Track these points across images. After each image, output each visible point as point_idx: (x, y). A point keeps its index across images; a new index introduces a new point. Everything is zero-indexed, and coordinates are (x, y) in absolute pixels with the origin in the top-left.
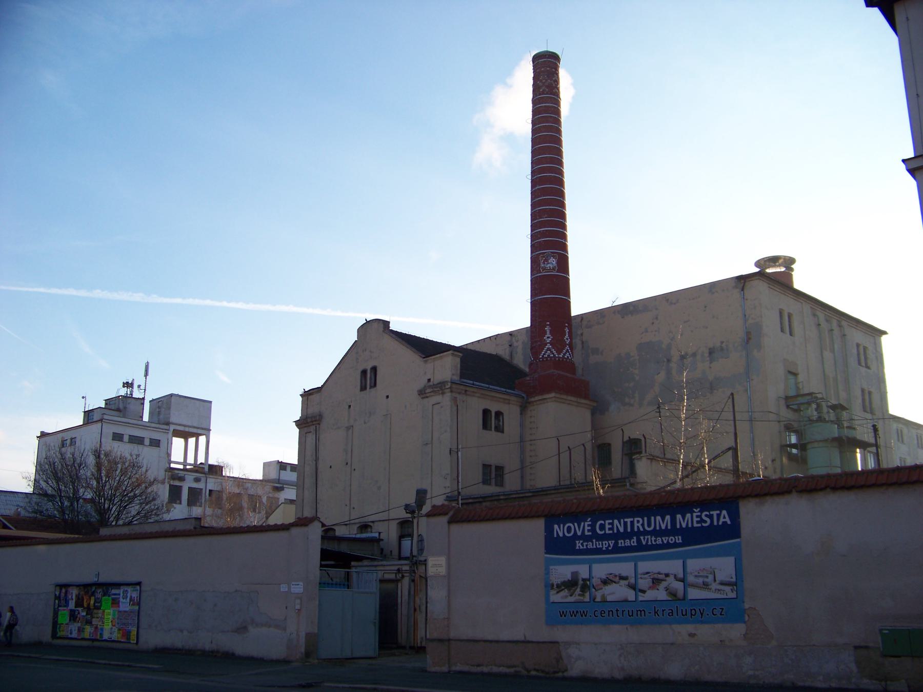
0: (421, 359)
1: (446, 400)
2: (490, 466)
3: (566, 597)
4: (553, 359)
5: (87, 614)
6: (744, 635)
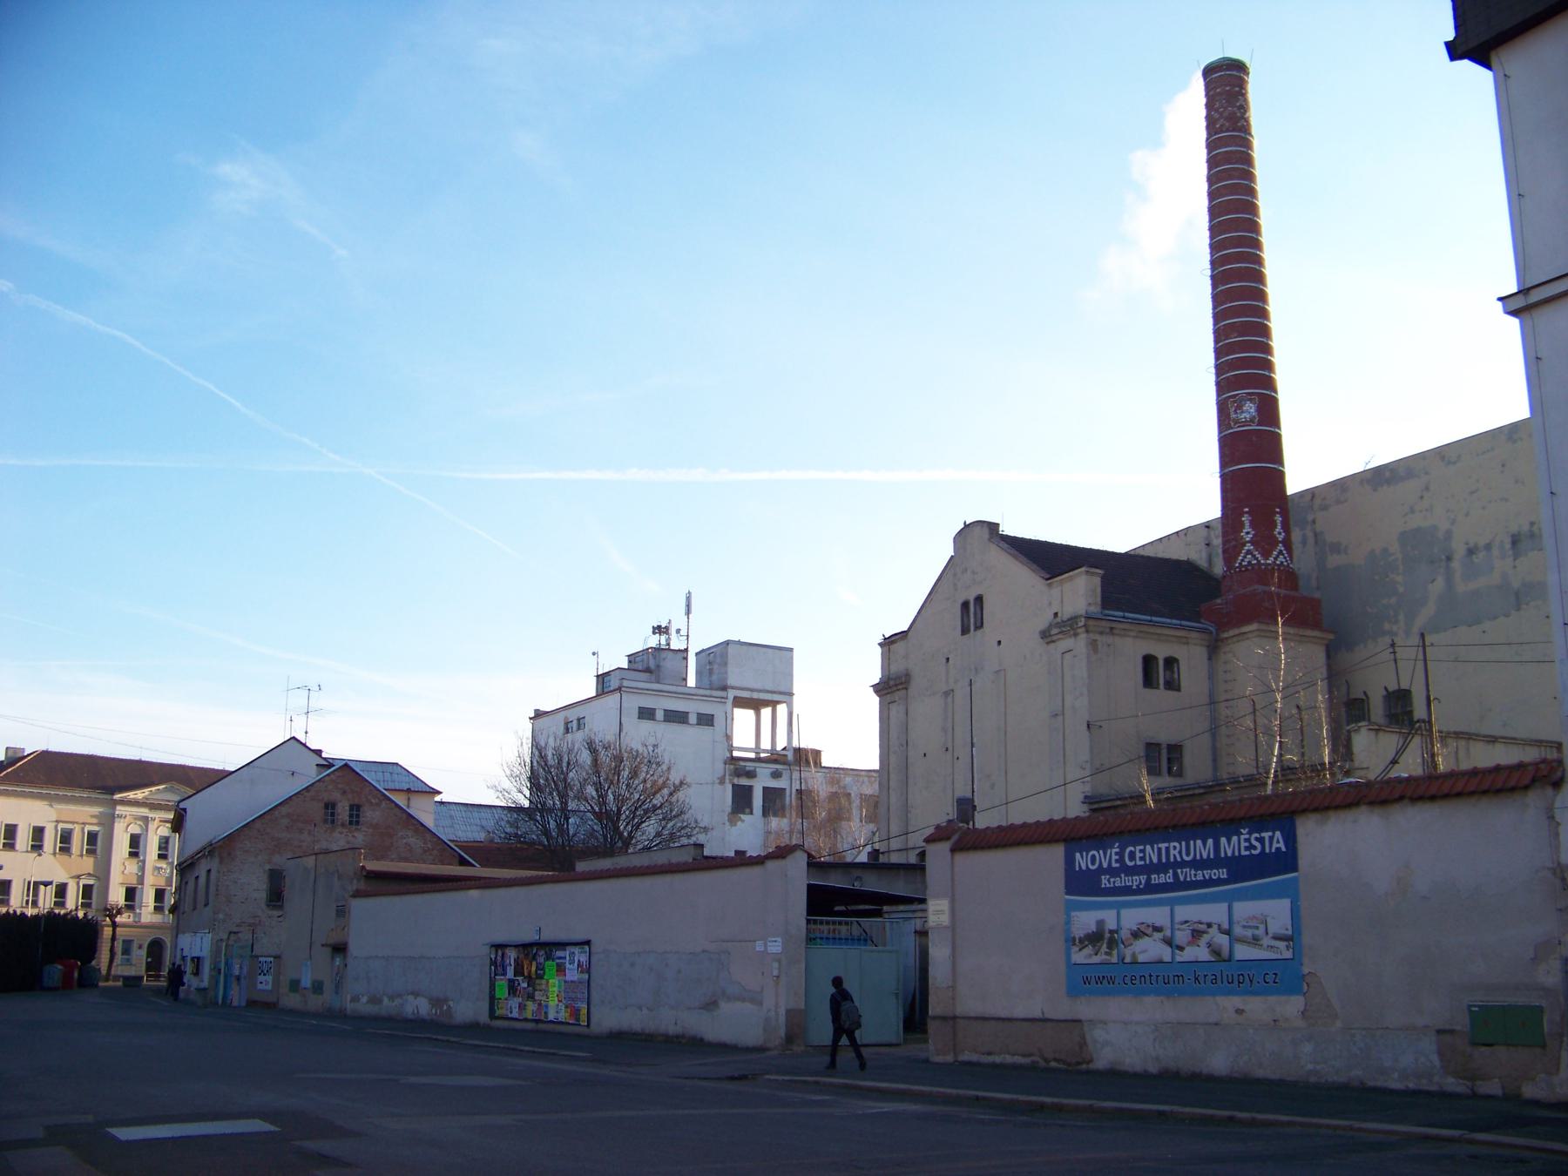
0: (1044, 581)
1: (1079, 644)
2: (1158, 745)
3: (1090, 956)
4: (1256, 567)
5: (528, 985)
6: (1302, 1013)
